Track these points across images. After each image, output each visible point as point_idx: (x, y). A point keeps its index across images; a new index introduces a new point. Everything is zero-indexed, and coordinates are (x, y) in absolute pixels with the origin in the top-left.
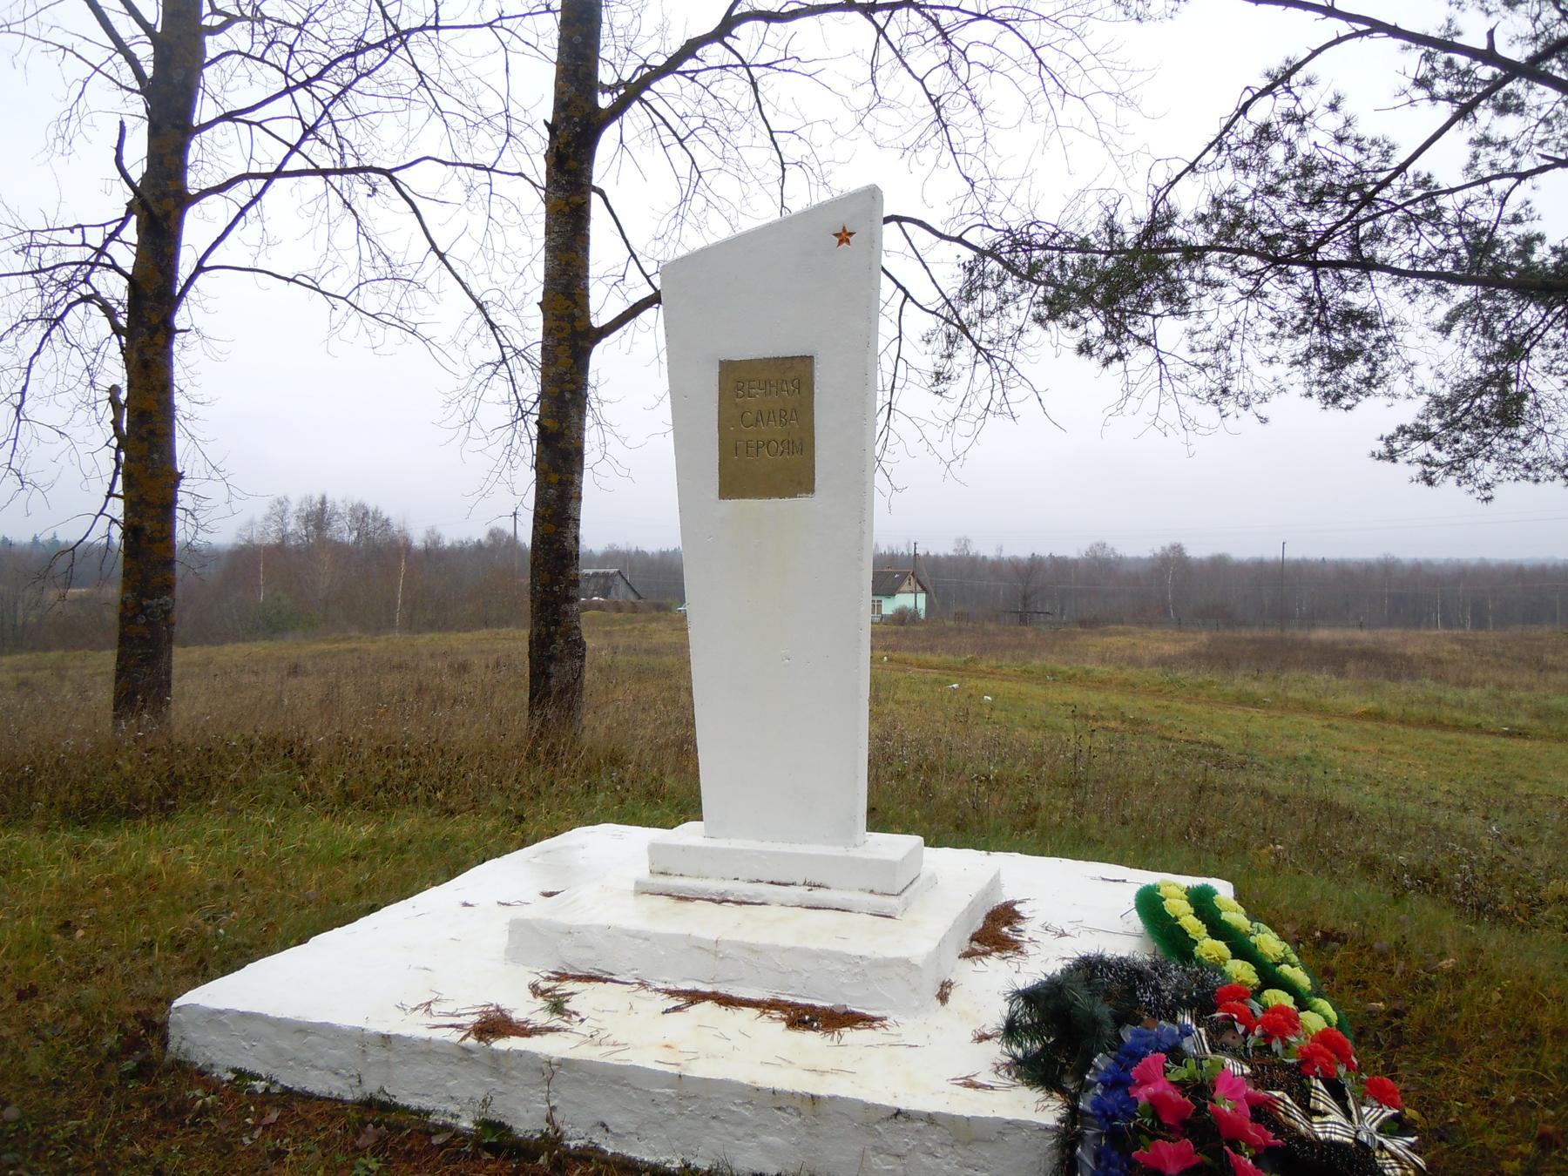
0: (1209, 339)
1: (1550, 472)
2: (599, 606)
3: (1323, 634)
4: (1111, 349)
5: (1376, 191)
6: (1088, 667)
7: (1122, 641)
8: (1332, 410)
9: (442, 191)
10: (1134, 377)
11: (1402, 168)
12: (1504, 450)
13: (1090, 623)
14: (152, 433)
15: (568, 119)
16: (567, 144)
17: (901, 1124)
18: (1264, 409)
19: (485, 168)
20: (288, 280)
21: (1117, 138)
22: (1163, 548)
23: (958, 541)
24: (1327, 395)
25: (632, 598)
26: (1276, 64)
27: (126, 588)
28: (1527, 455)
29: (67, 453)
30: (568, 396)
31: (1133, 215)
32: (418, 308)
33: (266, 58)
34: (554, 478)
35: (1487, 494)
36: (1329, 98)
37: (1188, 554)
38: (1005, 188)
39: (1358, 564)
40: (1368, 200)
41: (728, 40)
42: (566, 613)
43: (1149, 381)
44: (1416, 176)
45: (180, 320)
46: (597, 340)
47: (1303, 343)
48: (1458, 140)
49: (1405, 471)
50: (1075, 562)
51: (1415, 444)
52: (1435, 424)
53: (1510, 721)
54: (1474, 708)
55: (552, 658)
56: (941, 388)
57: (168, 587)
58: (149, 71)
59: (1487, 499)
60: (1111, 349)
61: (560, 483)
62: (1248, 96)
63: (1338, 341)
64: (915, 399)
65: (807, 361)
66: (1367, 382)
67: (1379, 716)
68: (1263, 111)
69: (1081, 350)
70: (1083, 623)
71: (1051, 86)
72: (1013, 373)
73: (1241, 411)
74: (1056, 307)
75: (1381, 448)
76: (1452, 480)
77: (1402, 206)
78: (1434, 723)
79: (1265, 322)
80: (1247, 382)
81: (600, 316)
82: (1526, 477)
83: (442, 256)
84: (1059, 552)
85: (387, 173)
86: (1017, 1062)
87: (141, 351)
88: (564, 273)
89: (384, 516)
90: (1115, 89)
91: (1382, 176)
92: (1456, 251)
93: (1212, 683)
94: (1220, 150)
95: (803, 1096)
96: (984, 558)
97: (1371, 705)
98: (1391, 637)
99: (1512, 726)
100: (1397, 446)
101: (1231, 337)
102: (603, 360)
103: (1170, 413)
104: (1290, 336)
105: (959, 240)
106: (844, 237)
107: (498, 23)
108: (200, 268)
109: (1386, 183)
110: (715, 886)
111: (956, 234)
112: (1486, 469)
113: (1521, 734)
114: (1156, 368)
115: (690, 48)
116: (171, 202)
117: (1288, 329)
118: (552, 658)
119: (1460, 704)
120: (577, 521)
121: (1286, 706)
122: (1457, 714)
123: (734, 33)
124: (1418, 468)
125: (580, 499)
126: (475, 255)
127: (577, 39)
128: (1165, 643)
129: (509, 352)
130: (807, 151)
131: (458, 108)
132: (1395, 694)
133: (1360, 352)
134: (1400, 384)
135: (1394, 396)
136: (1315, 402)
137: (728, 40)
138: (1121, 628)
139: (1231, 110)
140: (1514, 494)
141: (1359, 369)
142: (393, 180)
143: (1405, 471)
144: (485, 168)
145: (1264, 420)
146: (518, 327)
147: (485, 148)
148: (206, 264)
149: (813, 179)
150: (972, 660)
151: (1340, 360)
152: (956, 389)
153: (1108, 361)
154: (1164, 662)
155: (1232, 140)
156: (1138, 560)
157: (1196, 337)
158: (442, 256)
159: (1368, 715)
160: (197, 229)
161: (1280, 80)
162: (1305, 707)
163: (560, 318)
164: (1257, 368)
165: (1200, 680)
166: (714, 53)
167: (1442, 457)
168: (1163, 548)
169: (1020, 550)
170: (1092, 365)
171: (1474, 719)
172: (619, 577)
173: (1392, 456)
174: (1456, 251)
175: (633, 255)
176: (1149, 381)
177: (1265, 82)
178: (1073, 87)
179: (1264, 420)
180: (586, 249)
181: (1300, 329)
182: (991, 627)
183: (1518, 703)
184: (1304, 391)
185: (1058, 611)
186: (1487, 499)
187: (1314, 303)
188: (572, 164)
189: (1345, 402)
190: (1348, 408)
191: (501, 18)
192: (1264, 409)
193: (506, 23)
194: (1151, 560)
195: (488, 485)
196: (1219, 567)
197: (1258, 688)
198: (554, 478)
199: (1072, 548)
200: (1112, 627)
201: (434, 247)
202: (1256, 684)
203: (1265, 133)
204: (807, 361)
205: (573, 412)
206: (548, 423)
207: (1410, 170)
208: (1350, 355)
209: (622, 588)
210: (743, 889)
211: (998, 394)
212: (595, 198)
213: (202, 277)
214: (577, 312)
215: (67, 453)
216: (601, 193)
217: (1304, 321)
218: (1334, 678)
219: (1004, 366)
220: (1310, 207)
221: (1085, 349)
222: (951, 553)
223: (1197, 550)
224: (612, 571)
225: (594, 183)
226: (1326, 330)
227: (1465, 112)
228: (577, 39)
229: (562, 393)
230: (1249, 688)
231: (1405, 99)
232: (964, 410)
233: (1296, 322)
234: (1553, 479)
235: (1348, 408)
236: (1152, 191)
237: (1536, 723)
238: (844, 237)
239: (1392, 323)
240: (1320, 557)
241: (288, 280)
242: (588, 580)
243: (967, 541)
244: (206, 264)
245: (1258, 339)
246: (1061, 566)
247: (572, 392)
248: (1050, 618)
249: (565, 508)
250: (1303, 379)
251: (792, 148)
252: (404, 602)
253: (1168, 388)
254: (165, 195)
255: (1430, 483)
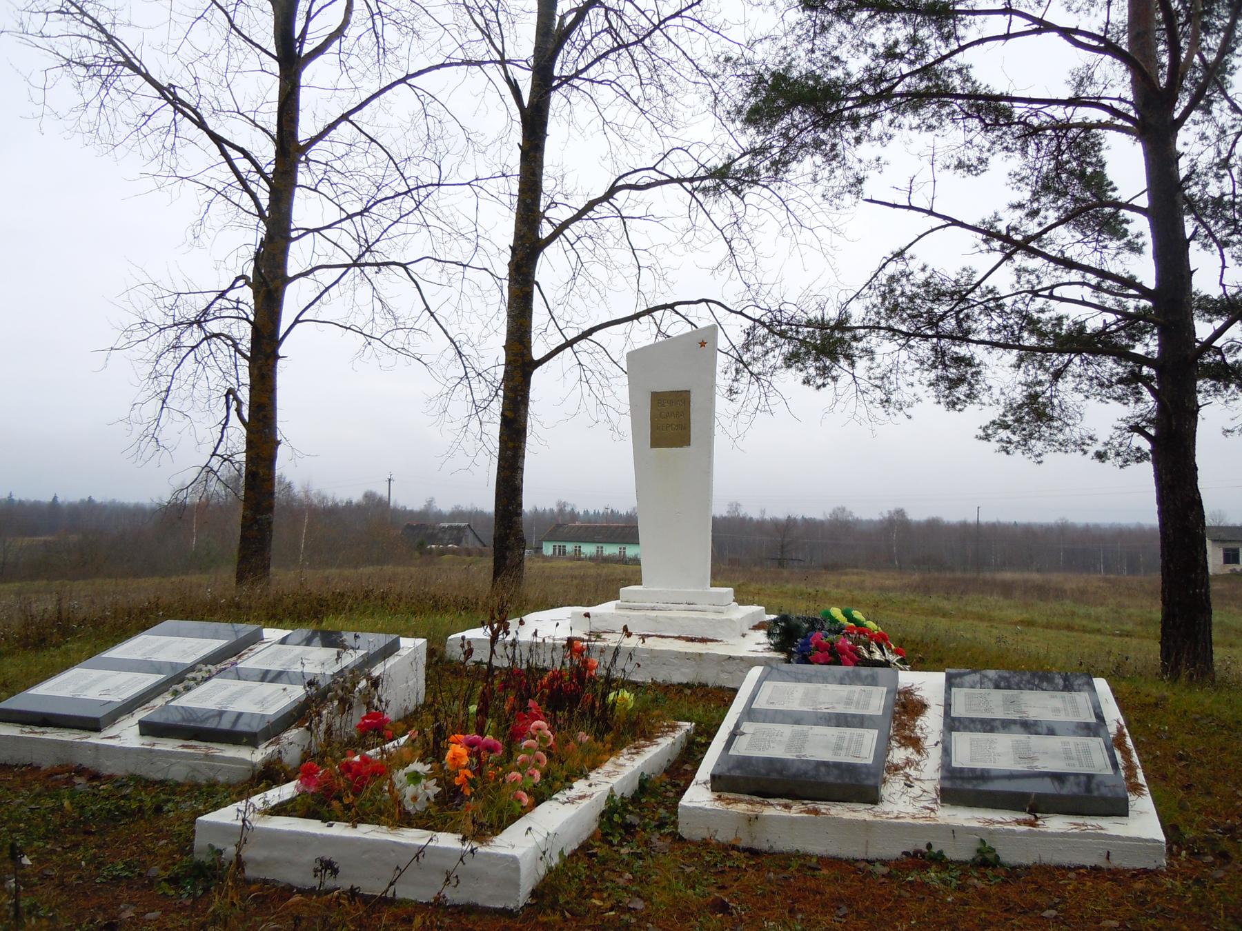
0: (878, 372)
1: (1073, 447)
2: (453, 552)
3: (1008, 576)
4: (820, 381)
5: (966, 295)
6: (827, 589)
7: (855, 578)
8: (952, 412)
9: (427, 272)
10: (840, 391)
11: (978, 284)
12: (1047, 435)
13: (832, 567)
14: (265, 416)
15: (523, 245)
16: (522, 259)
17: (731, 661)
18: (909, 411)
19: (462, 265)
20: (347, 328)
21: (830, 250)
22: (889, 512)
23: (730, 505)
24: (948, 403)
25: (479, 545)
26: (897, 250)
27: (245, 508)
28: (1060, 437)
29: (187, 429)
30: (519, 398)
31: (832, 314)
32: (418, 344)
33: (319, 188)
34: (511, 445)
35: (1039, 459)
36: (921, 266)
37: (909, 518)
38: (766, 289)
39: (1041, 526)
40: (963, 299)
41: (611, 200)
42: (515, 522)
43: (850, 393)
44: (987, 287)
45: (281, 352)
46: (536, 367)
47: (932, 375)
48: (1007, 270)
49: (994, 445)
50: (822, 523)
51: (1000, 431)
52: (1010, 419)
53: (1121, 627)
54: (1097, 619)
55: (507, 548)
56: (732, 397)
57: (270, 508)
58: (265, 203)
59: (1039, 462)
60: (820, 381)
61: (514, 447)
62: (885, 261)
63: (953, 372)
64: (721, 403)
65: (688, 392)
66: (968, 396)
67: (1030, 623)
68: (892, 269)
69: (804, 383)
70: (826, 567)
71: (793, 221)
72: (771, 388)
73: (896, 412)
74: (792, 359)
75: (982, 434)
76: (1019, 451)
77: (981, 303)
78: (1070, 628)
79: (913, 362)
80: (900, 396)
81: (537, 354)
82: (1060, 450)
83: (432, 314)
84: (810, 514)
85: (404, 266)
86: (775, 645)
87: (260, 369)
88: (519, 329)
89: (287, 480)
90: (830, 225)
91: (970, 287)
92: (1011, 327)
93: (914, 601)
94: (870, 288)
95: (696, 654)
96: (751, 519)
97: (1025, 616)
98: (1056, 578)
99: (1122, 631)
100: (990, 432)
101: (891, 371)
102: (538, 378)
103: (862, 411)
104: (927, 370)
105: (741, 313)
106: (703, 344)
107: (475, 183)
108: (297, 321)
109: (972, 290)
110: (649, 605)
111: (739, 310)
112: (1038, 446)
113: (1129, 634)
114: (853, 387)
115: (590, 206)
116: (278, 282)
117: (926, 366)
118: (507, 548)
119: (1088, 616)
120: (522, 469)
121: (965, 616)
122: (1085, 622)
123: (615, 196)
124: (999, 445)
125: (524, 457)
126: (452, 314)
127: (529, 201)
128: (888, 579)
129: (472, 374)
130: (655, 262)
131: (437, 223)
132: (1042, 610)
133: (964, 380)
134: (985, 398)
135: (984, 404)
136: (942, 407)
137: (611, 200)
138: (855, 570)
139: (876, 268)
140: (1053, 459)
141: (964, 389)
142: (406, 269)
143: (994, 445)
144: (462, 265)
145: (910, 417)
146: (476, 356)
147: (460, 250)
148: (300, 319)
149: (657, 276)
150: (743, 584)
151: (954, 383)
152: (740, 398)
153: (818, 387)
154: (883, 589)
155: (876, 283)
156: (870, 522)
157: (872, 371)
158: (432, 314)
159: (1022, 622)
160: (294, 298)
161: (899, 255)
162: (980, 618)
163: (516, 355)
164: (904, 387)
165: (905, 598)
166: (603, 209)
167: (1015, 438)
168: (889, 512)
169: (778, 511)
170: (811, 389)
171: (1096, 626)
172: (468, 530)
173: (987, 437)
174: (1011, 327)
175: (553, 318)
176: (850, 393)
177: (891, 256)
178: (806, 223)
179: (910, 417)
180: (530, 317)
181: (933, 366)
182: (757, 569)
183: (1130, 616)
184: (936, 400)
185: (808, 560)
186: (1039, 462)
187: (939, 353)
188: (525, 269)
189: (958, 407)
190: (960, 410)
191: (477, 179)
192: (909, 411)
193: (480, 183)
194: (881, 522)
195: (452, 451)
196: (933, 528)
197: (946, 605)
198: (511, 445)
199: (819, 512)
200: (848, 570)
201: (428, 308)
202: (946, 602)
203: (892, 279)
204: (688, 392)
205: (522, 407)
206: (507, 413)
207: (982, 285)
208: (961, 380)
209: (471, 536)
210: (660, 605)
211: (763, 399)
212: (535, 287)
213: (298, 325)
214: (525, 351)
215: (187, 429)
216: (537, 284)
217: (934, 362)
218: (1001, 599)
219: (766, 384)
220: (933, 301)
221: (807, 381)
222: (725, 514)
223: (917, 514)
224: (463, 524)
225: (536, 279)
226: (945, 366)
227: (1008, 257)
228: (529, 201)
229: (516, 396)
230: (940, 605)
231: (977, 249)
232: (744, 409)
233: (930, 362)
234: (1075, 451)
235: (960, 410)
236: (839, 304)
237: (1139, 628)
238: (703, 344)
239: (979, 365)
240: (1012, 521)
241: (347, 328)
242: (444, 532)
243: (738, 505)
244: (300, 319)
245: (905, 372)
246: (810, 525)
247: (521, 396)
248: (802, 563)
249: (516, 462)
250: (934, 394)
251: (644, 259)
252: (306, 547)
253: (861, 397)
254: (276, 278)
255: (1008, 453)
